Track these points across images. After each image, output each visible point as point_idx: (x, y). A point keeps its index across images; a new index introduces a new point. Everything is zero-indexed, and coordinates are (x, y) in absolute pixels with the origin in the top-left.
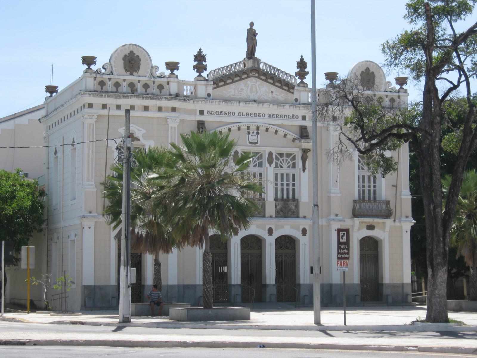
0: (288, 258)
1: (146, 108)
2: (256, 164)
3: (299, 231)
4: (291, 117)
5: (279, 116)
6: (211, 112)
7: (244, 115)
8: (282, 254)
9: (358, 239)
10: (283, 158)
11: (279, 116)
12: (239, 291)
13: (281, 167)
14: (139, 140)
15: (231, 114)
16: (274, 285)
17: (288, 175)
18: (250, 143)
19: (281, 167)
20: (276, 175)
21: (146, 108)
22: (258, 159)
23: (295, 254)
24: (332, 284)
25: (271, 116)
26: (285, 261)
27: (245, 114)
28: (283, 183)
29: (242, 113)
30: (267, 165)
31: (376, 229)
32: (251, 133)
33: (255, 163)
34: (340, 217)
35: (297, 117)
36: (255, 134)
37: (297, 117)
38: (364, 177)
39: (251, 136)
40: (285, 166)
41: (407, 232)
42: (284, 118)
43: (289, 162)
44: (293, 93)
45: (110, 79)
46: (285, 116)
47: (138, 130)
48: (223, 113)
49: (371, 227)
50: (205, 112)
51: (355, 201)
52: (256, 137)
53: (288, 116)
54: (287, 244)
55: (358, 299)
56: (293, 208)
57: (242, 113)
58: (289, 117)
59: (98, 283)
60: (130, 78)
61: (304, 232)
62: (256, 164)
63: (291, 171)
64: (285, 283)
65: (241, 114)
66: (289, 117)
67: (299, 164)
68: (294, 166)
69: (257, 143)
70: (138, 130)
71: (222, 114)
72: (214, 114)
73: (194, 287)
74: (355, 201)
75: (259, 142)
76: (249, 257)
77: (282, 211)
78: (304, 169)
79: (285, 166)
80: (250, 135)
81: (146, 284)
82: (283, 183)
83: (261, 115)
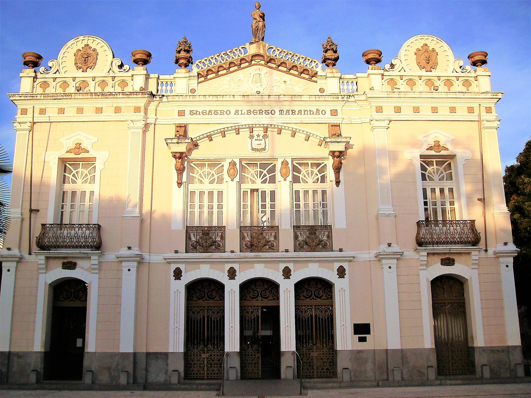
0: (321, 312)
1: (99, 110)
2: (267, 179)
3: (333, 271)
4: (315, 113)
5: (297, 113)
6: (195, 112)
7: (243, 113)
8: (311, 306)
9: (427, 280)
10: (77, 171)
11: (297, 113)
12: (236, 362)
13: (201, 182)
14: (88, 152)
15: (225, 113)
16: (293, 353)
17: (211, 193)
18: (253, 149)
19: (201, 182)
20: (425, 190)
21: (99, 110)
22: (269, 172)
23: (464, 303)
24: (387, 350)
25: (285, 113)
26: (316, 316)
27: (245, 111)
28: (427, 202)
29: (241, 111)
30: (281, 179)
31: (456, 264)
32: (256, 137)
33: (442, 175)
34: (395, 248)
35: (324, 112)
36: (261, 138)
37: (324, 112)
38: (297, 192)
39: (256, 140)
40: (310, 180)
41: (507, 266)
42: (305, 114)
43: (442, 173)
44: (316, 82)
45: (55, 79)
46: (306, 112)
47: (87, 138)
48: (213, 112)
49: (448, 262)
50: (187, 112)
51: (419, 224)
52: (263, 142)
53: (310, 111)
54: (315, 292)
55: (432, 374)
56: (218, 239)
57: (241, 111)
58: (312, 112)
59: (404, 348)
60: (79, 74)
61: (341, 272)
62: (267, 179)
63: (319, 186)
64: (317, 349)
65: (240, 112)
66: (312, 112)
67: (330, 174)
68: (323, 179)
69: (264, 149)
70: (87, 138)
71: (319, 114)
72: (199, 114)
73: (508, 350)
74: (419, 224)
75: (267, 148)
76: (313, 310)
77: (306, 243)
78: (338, 183)
79: (206, 181)
80: (254, 140)
81: (475, 345)
82: (427, 202)
83: (270, 112)
